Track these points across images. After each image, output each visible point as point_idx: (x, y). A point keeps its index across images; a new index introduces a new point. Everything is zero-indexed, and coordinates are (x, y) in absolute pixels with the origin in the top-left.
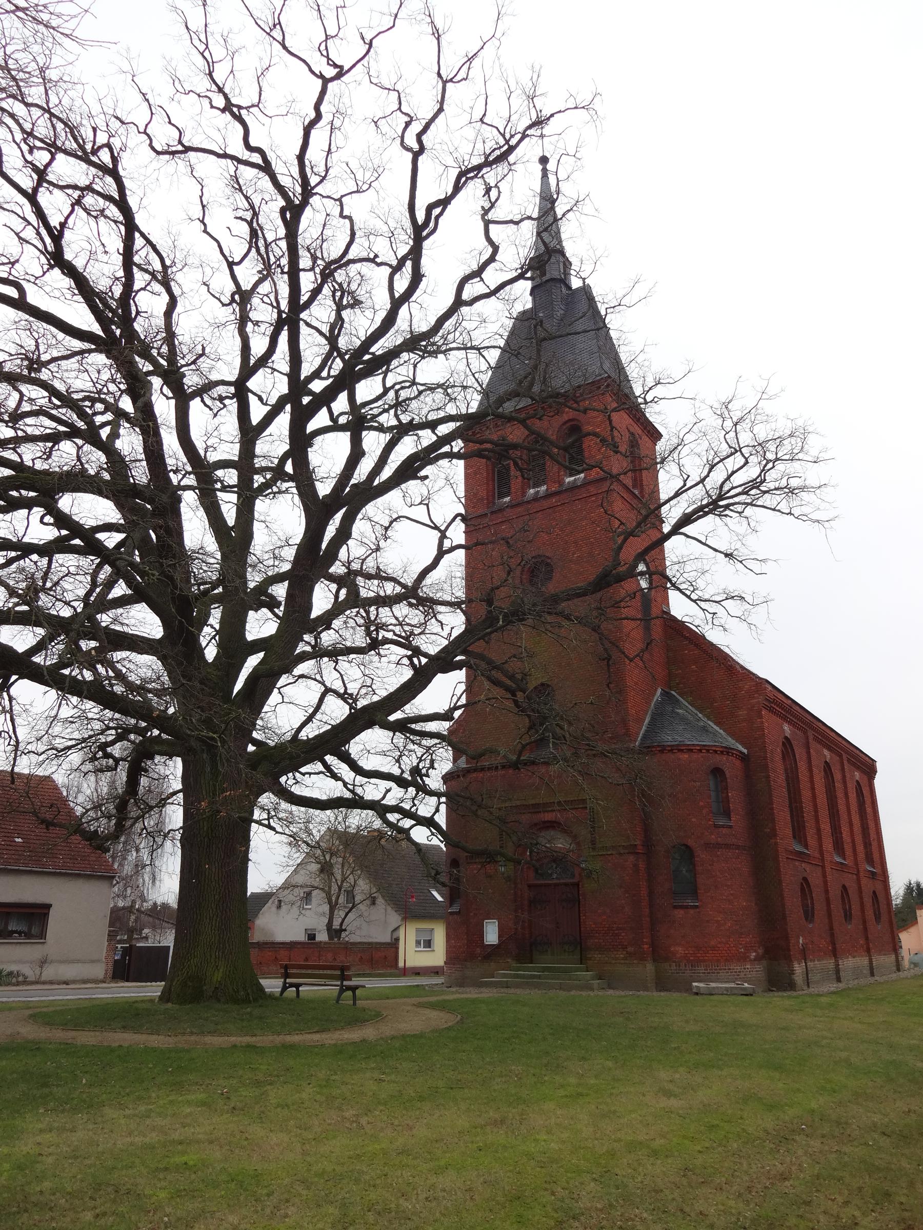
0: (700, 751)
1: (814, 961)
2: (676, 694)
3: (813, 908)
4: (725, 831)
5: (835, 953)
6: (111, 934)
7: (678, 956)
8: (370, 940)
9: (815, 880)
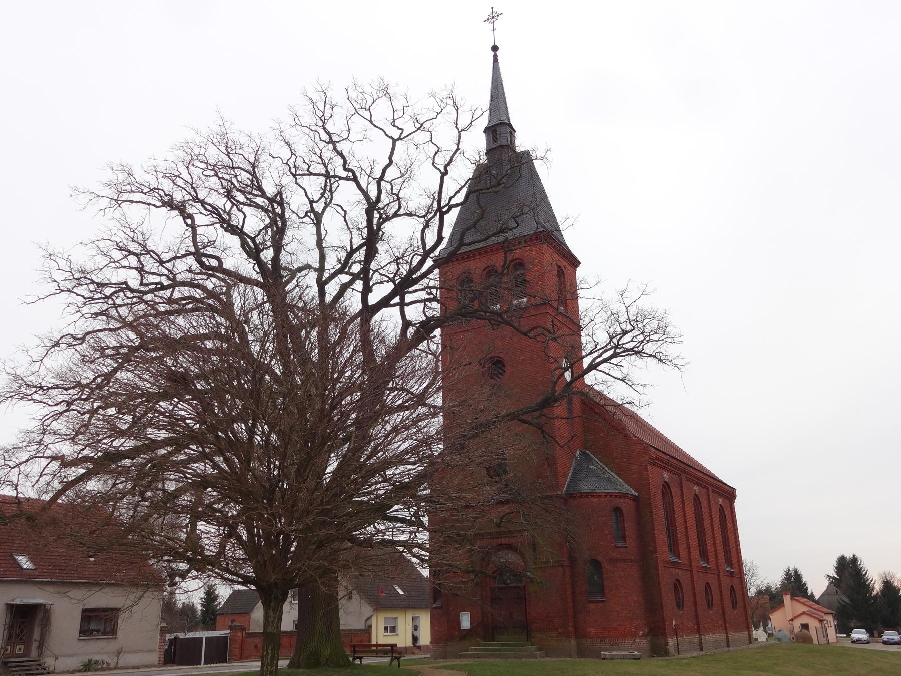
3: (683, 601)
4: (622, 550)
5: (699, 631)
6: (163, 629)
7: (591, 634)
8: (349, 628)
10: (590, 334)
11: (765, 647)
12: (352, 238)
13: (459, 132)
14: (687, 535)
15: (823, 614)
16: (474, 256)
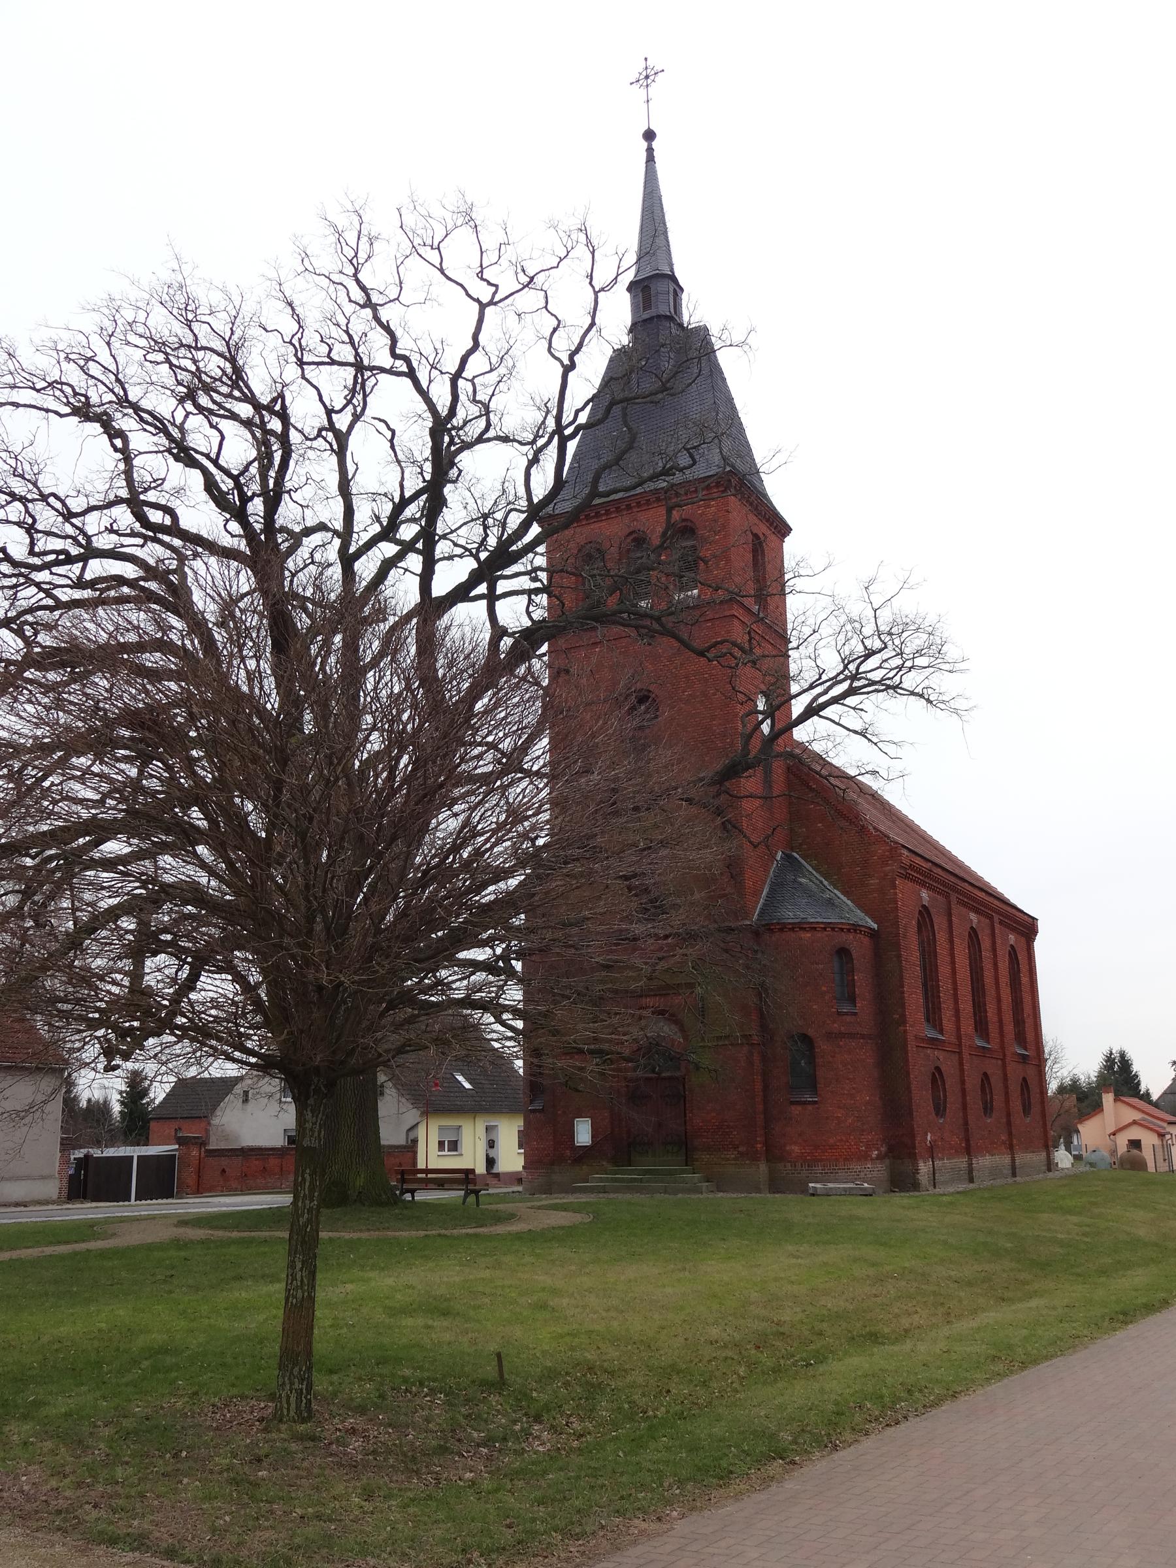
0: (825, 929)
1: (943, 1159)
2: (798, 856)
4: (848, 1019)
5: (968, 1151)
9: (949, 1066)
10: (813, 657)
11: (1071, 1178)
12: (403, 479)
13: (596, 293)
14: (955, 996)
15: (1165, 1125)
16: (608, 512)
